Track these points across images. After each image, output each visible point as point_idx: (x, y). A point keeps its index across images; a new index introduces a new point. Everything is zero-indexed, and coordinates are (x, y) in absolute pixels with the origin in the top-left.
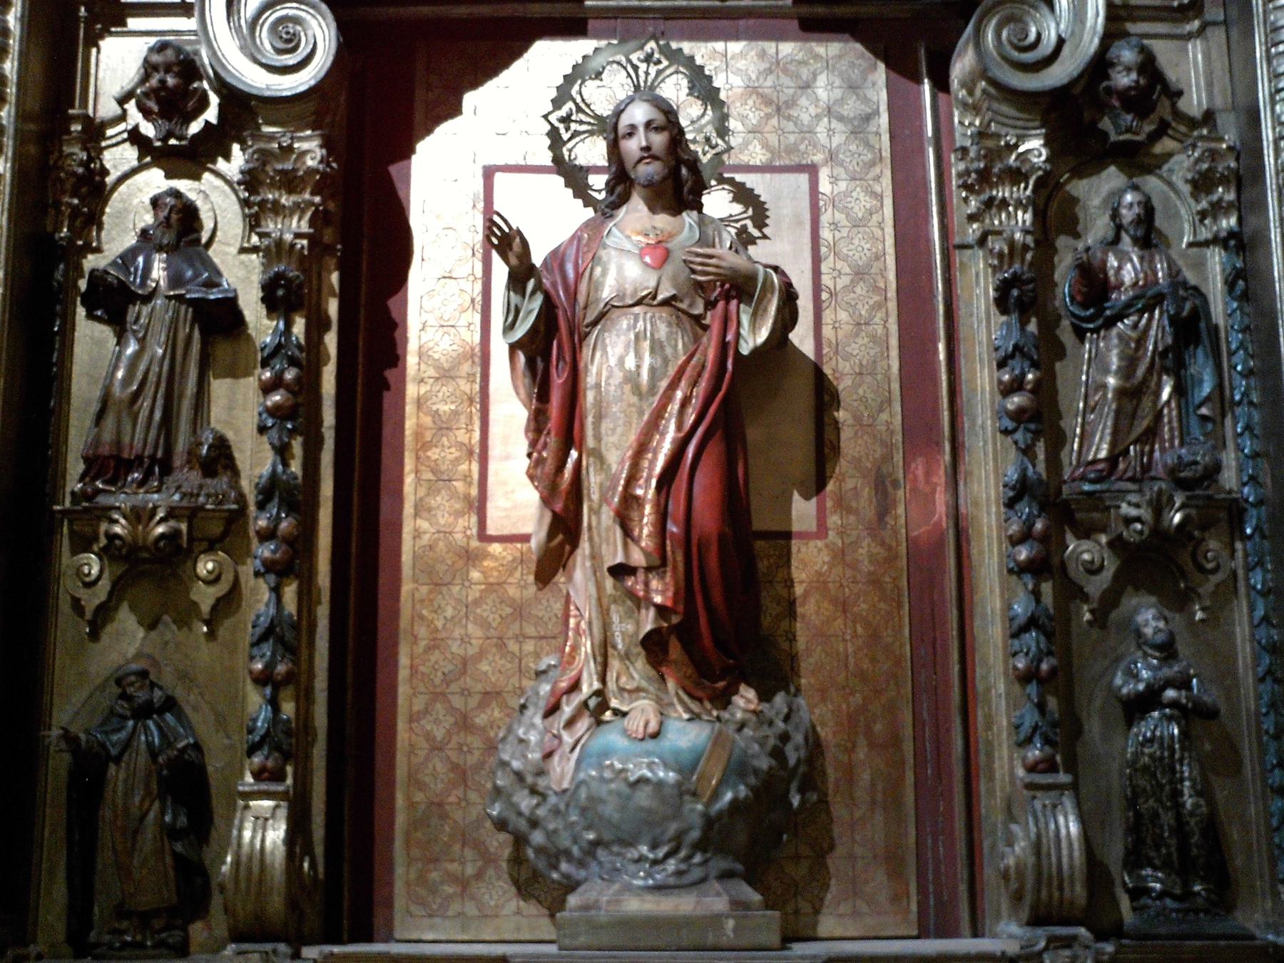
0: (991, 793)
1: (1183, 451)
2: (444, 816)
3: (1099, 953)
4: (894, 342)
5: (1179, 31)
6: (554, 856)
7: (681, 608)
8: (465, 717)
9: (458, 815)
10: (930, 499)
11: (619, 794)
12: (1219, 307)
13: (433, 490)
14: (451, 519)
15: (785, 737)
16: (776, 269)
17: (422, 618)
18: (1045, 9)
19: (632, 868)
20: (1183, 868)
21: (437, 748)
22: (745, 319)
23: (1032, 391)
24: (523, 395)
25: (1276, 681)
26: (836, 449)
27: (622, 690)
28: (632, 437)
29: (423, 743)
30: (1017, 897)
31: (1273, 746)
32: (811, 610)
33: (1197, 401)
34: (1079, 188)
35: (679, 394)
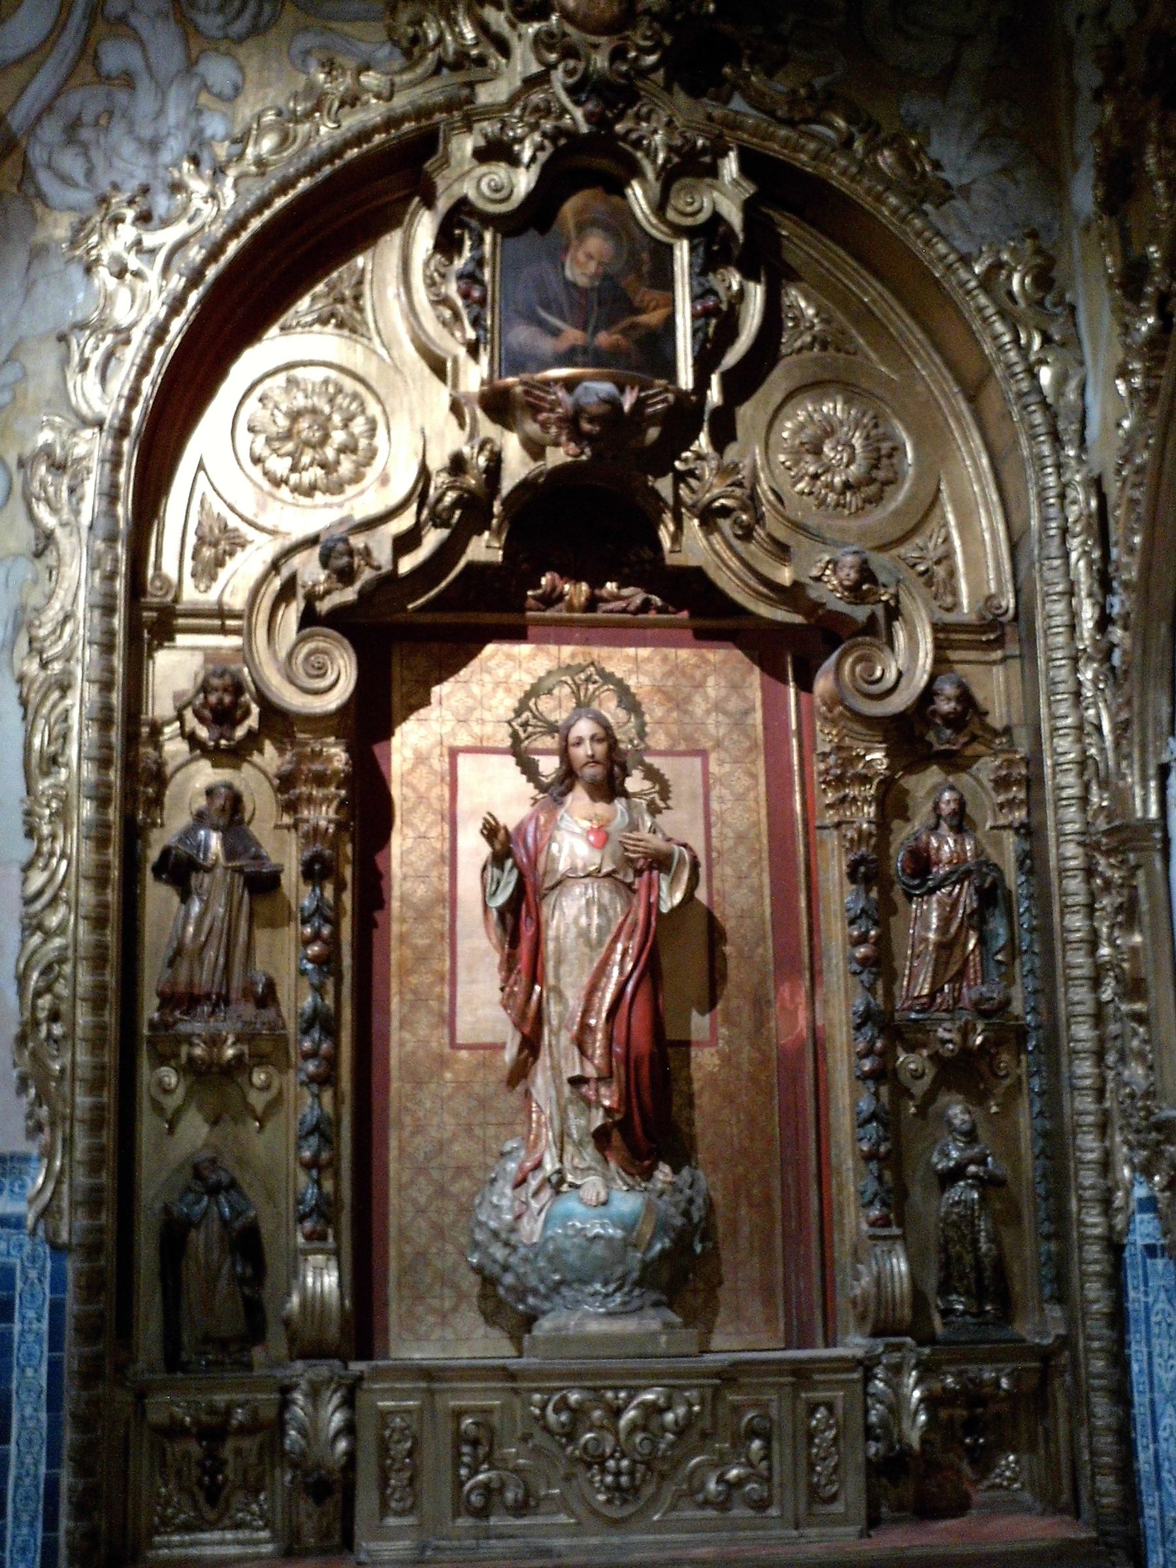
0: (842, 1240)
1: (984, 989)
2: (428, 1264)
3: (919, 1354)
4: (767, 891)
5: (987, 658)
6: (522, 1293)
7: (623, 1109)
8: (442, 1187)
9: (438, 1263)
10: (794, 1014)
11: (580, 1246)
12: (1013, 879)
13: (414, 1007)
14: (427, 1032)
15: (691, 1201)
16: (685, 846)
17: (407, 1109)
18: (887, 650)
19: (590, 1299)
20: (979, 1294)
21: (421, 1211)
22: (664, 886)
23: (875, 944)
24: (494, 940)
25: (1047, 1158)
26: (724, 977)
27: (576, 1168)
28: (586, 980)
29: (410, 1208)
30: (862, 1318)
31: (1043, 1206)
32: (704, 1101)
33: (995, 949)
34: (910, 782)
35: (620, 947)
